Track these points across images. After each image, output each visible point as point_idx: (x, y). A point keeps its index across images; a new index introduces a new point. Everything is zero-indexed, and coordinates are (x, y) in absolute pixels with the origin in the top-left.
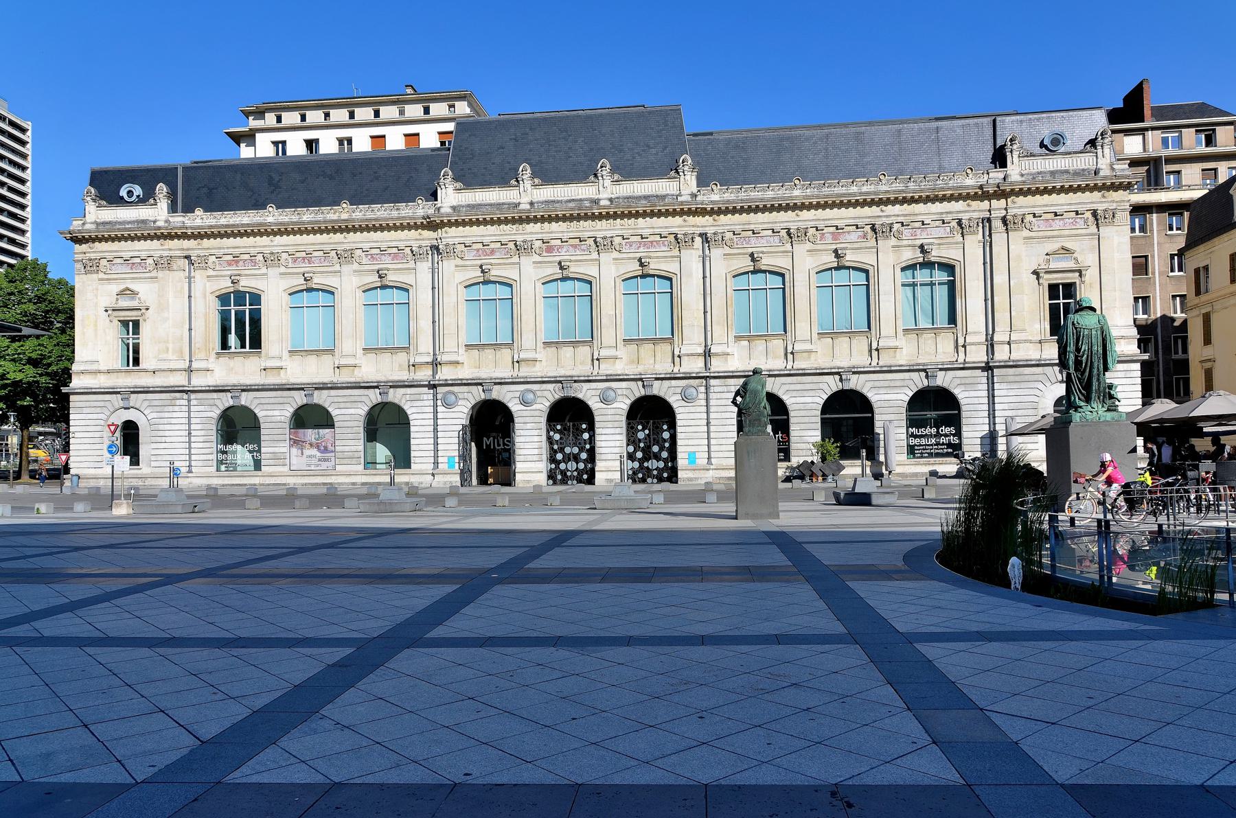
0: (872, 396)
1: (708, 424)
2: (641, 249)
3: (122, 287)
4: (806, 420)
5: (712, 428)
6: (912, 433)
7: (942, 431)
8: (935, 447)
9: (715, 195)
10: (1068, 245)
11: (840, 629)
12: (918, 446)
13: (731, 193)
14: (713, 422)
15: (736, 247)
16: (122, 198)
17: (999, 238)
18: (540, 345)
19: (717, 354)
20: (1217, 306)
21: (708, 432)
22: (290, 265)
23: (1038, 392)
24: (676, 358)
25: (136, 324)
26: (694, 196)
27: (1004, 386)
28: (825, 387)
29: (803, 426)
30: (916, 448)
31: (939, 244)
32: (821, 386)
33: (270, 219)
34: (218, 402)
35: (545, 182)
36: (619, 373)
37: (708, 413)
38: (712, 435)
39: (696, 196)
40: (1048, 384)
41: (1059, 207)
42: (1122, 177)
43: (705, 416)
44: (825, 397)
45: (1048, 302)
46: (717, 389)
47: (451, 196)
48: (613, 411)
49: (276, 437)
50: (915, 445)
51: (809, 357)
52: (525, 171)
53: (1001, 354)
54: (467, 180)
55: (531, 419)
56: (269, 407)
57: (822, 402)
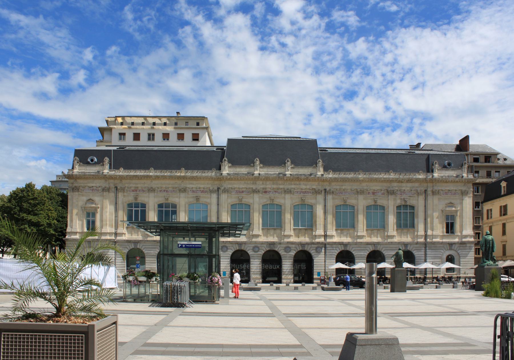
2: (301, 194)
3: (88, 198)
10: (453, 201)
11: (283, 326)
16: (89, 162)
17: (430, 198)
20: (495, 224)
23: (441, 253)
26: (322, 175)
27: (430, 251)
28: (368, 249)
32: (367, 248)
34: (128, 247)
40: (445, 250)
46: (329, 249)
47: (226, 170)
49: (152, 262)
54: (234, 163)
55: (257, 258)
56: (150, 249)
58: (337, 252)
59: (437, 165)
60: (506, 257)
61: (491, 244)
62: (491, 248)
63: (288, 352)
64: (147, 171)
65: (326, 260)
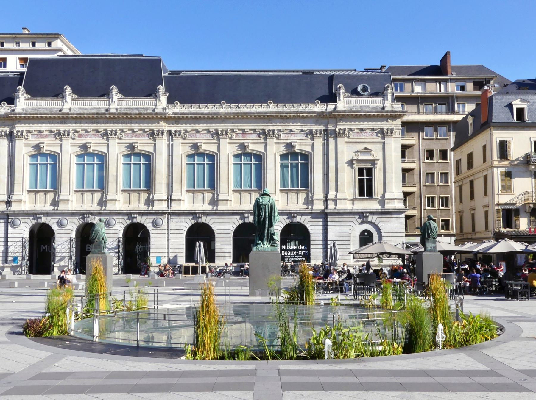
0: (214, 227)
1: (168, 240)
2: (134, 138)
4: (224, 239)
5: (171, 243)
6: (283, 248)
7: (300, 247)
8: (295, 257)
9: (179, 109)
10: (369, 147)
12: (286, 256)
13: (279, 107)
14: (171, 239)
15: (188, 139)
17: (331, 141)
18: (231, 192)
19: (175, 201)
21: (168, 245)
22: (123, 138)
23: (350, 227)
24: (149, 202)
25: (369, 172)
26: (164, 109)
29: (222, 243)
30: (285, 257)
31: (301, 143)
32: (233, 220)
33: (222, 110)
35: (33, 97)
36: (118, 209)
37: (168, 233)
38: (170, 247)
39: (166, 109)
41: (364, 126)
42: (397, 112)
43: (166, 235)
44: (235, 227)
45: (357, 178)
48: (113, 232)
50: (285, 255)
51: (227, 204)
52: (115, 90)
53: (331, 206)
57: (233, 230)
58: (188, 227)
59: (342, 91)
60: (475, 233)
61: (267, 211)
62: (267, 219)
63: (421, 384)
64: (217, 105)
65: (170, 238)
